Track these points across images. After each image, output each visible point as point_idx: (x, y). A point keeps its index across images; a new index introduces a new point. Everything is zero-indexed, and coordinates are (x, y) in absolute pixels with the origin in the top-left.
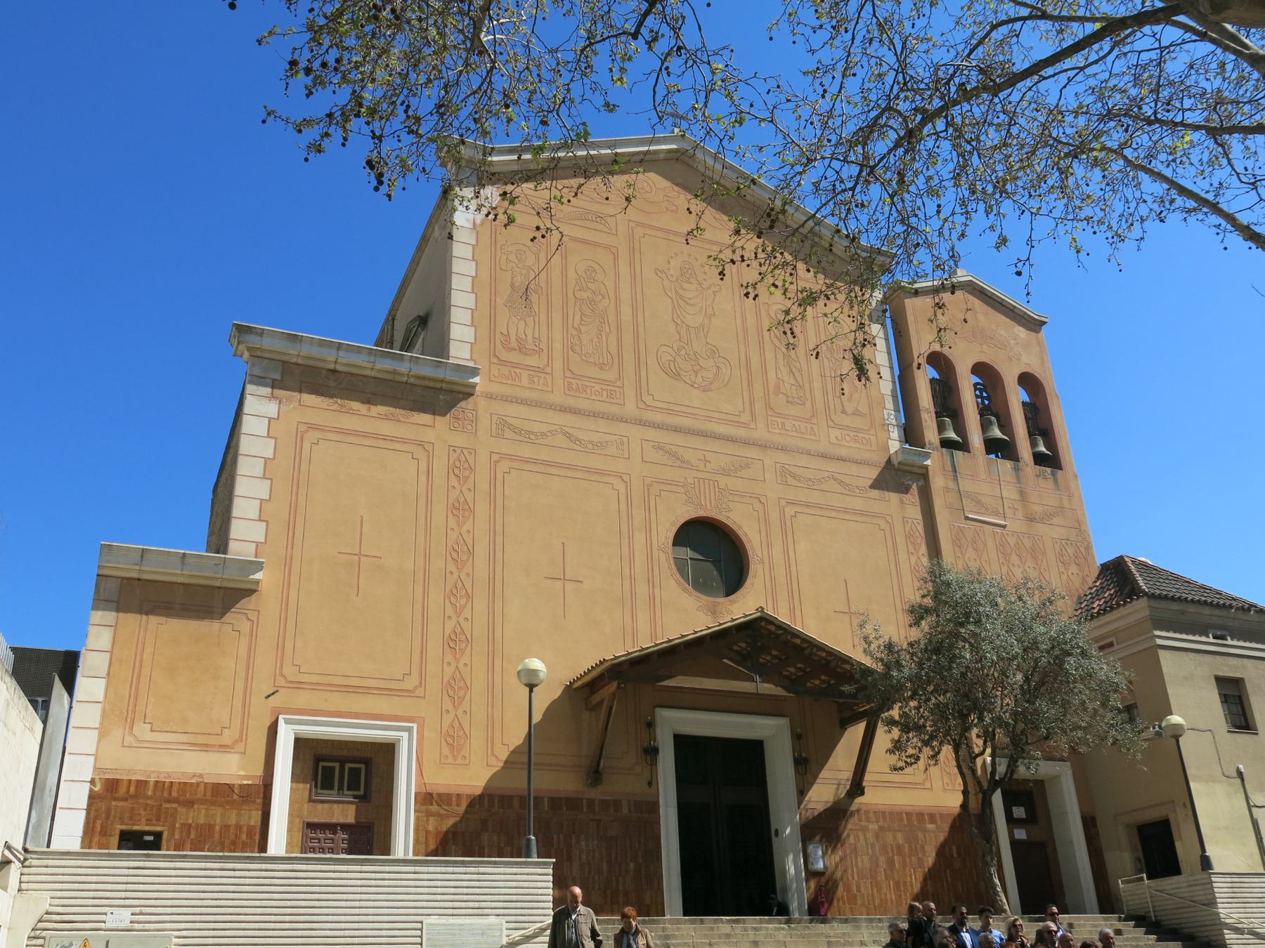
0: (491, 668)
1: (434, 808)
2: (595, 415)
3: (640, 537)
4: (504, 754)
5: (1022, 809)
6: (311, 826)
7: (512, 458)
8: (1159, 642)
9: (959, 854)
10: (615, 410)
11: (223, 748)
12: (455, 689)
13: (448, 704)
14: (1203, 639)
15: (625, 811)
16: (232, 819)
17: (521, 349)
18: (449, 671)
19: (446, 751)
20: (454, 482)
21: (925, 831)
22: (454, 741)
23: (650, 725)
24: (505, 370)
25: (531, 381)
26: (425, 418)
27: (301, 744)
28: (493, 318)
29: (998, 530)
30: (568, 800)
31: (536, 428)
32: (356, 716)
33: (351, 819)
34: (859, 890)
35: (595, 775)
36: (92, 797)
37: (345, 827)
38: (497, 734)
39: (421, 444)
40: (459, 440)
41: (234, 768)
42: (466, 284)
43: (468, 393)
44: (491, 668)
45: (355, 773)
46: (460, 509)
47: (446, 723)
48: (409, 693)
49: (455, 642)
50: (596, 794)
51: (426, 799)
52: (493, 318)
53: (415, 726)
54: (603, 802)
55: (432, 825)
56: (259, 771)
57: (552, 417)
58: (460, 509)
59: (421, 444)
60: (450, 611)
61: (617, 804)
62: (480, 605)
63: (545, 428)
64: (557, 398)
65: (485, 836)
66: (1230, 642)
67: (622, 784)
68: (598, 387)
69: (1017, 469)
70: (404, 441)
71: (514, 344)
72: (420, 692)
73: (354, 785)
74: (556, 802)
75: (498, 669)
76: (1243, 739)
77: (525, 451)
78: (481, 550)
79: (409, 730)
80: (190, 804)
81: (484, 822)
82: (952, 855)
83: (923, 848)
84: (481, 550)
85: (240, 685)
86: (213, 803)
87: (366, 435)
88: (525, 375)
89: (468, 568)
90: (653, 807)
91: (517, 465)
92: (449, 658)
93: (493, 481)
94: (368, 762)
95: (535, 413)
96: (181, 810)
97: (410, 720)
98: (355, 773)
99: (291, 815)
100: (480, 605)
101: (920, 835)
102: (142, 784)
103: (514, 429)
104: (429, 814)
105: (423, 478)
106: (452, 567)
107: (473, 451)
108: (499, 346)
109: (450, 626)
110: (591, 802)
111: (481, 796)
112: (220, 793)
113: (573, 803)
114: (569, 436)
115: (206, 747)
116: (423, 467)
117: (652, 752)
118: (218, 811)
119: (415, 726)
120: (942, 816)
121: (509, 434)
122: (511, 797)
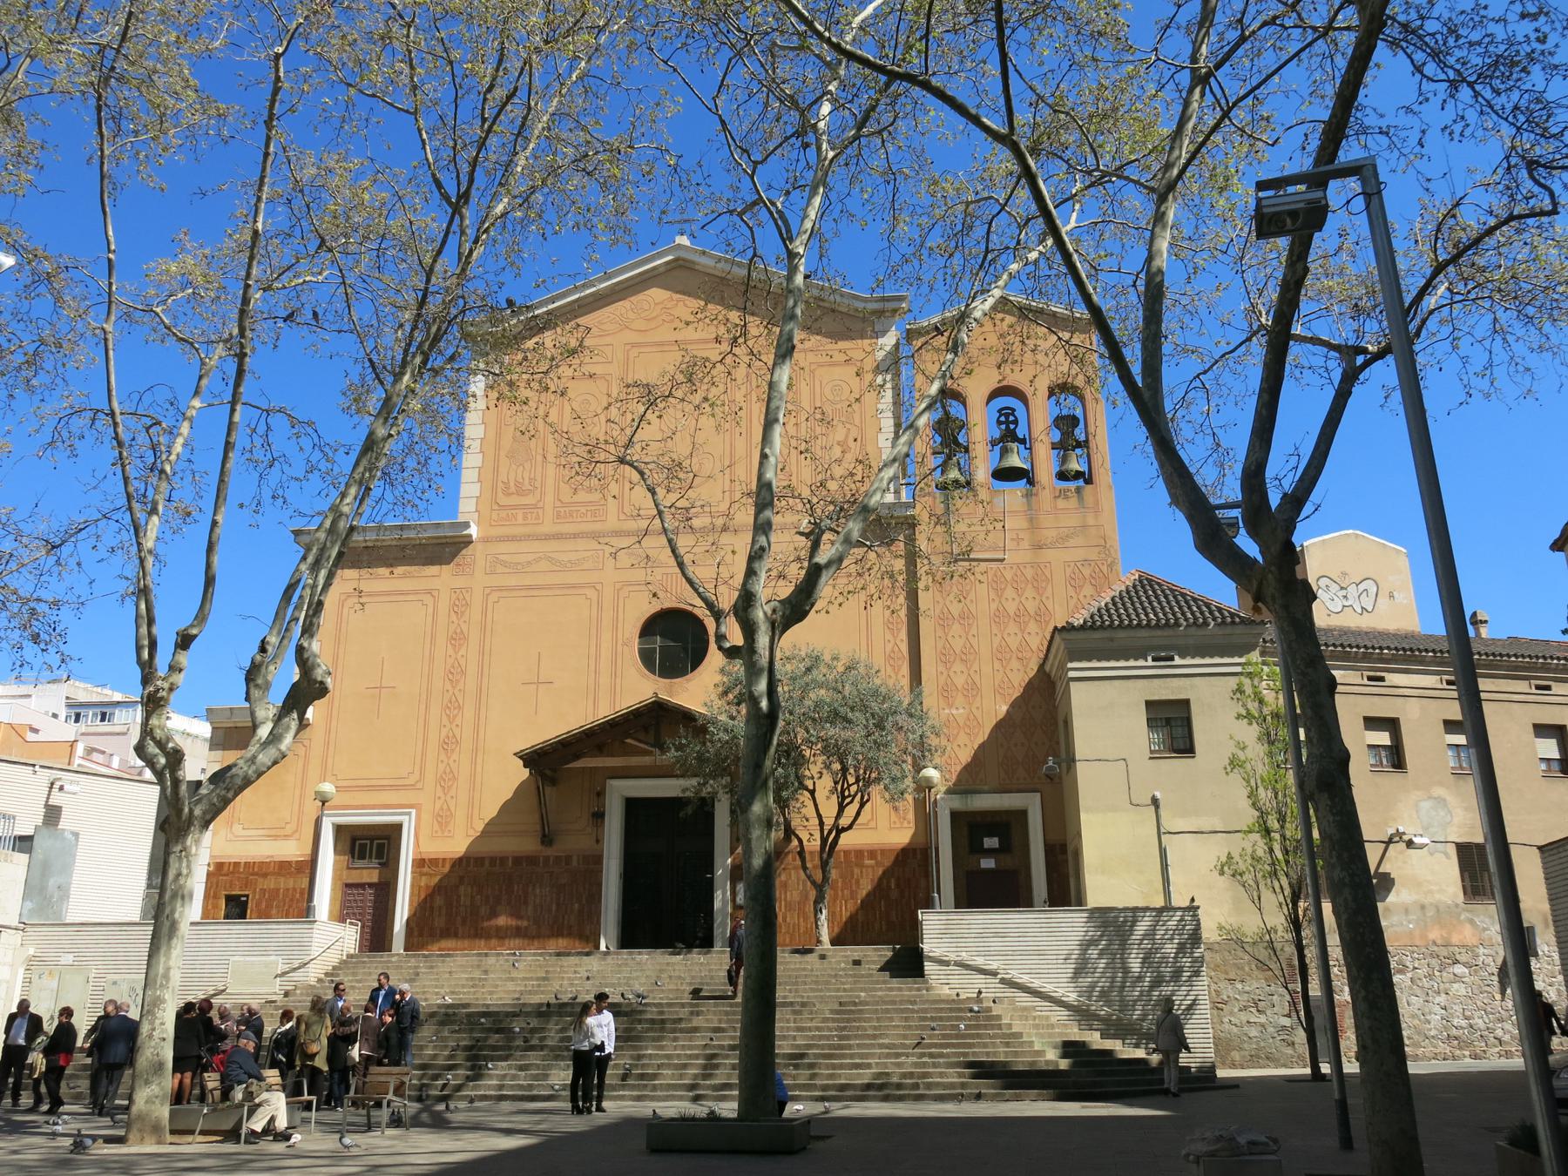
0: (474, 762)
1: (426, 869)
2: (575, 536)
3: (606, 637)
4: (480, 827)
5: (996, 840)
6: (347, 885)
7: (500, 589)
8: (1072, 674)
9: (898, 885)
10: (597, 527)
11: (286, 837)
12: (446, 781)
13: (440, 793)
14: (1141, 663)
15: (575, 863)
16: (291, 883)
17: (520, 492)
18: (997, 641)
19: (436, 827)
20: (454, 617)
21: (862, 866)
22: (443, 820)
23: (600, 794)
24: (503, 514)
25: (525, 518)
26: (434, 569)
27: (339, 830)
28: (496, 470)
29: (994, 565)
30: (528, 858)
31: (523, 558)
32: (373, 807)
33: (375, 879)
34: (784, 920)
35: (547, 839)
36: (209, 874)
37: (371, 885)
38: (476, 811)
39: (429, 592)
40: (459, 582)
41: (293, 850)
42: (476, 445)
43: (467, 541)
44: (474, 762)
45: (381, 847)
46: (458, 639)
47: (438, 806)
48: (412, 787)
49: (449, 744)
50: (550, 852)
51: (420, 863)
52: (496, 470)
53: (414, 812)
54: (557, 857)
55: (424, 881)
56: (309, 851)
57: (536, 546)
58: (458, 639)
59: (429, 592)
60: (445, 721)
61: (568, 859)
62: (469, 713)
63: (530, 557)
64: (547, 528)
65: (462, 889)
66: (1178, 661)
67: (573, 842)
68: (583, 510)
69: (1028, 495)
70: (416, 592)
71: (513, 489)
72: (419, 785)
73: (379, 855)
74: (518, 860)
75: (479, 761)
76: (1180, 764)
77: (512, 581)
78: (472, 670)
79: (409, 814)
80: (265, 875)
81: (461, 878)
82: (889, 887)
83: (858, 882)
84: (472, 670)
85: (298, 792)
86: (279, 874)
87: (388, 593)
88: (520, 514)
89: (461, 686)
90: (598, 859)
91: (505, 594)
92: (443, 757)
93: (484, 613)
94: (388, 838)
95: (524, 546)
96: (261, 880)
97: (411, 806)
98: (381, 847)
99: (334, 879)
100: (469, 713)
101: (857, 871)
102: (237, 864)
103: (504, 564)
104: (422, 874)
105: (430, 619)
106: (448, 686)
107: (469, 589)
108: (500, 494)
109: (444, 732)
110: (547, 859)
111: (460, 859)
112: (283, 867)
113: (531, 860)
114: (550, 559)
115: (276, 837)
116: (430, 610)
117: (599, 816)
118: (282, 880)
119: (414, 812)
120: (883, 851)
121: (500, 569)
122: (483, 859)
